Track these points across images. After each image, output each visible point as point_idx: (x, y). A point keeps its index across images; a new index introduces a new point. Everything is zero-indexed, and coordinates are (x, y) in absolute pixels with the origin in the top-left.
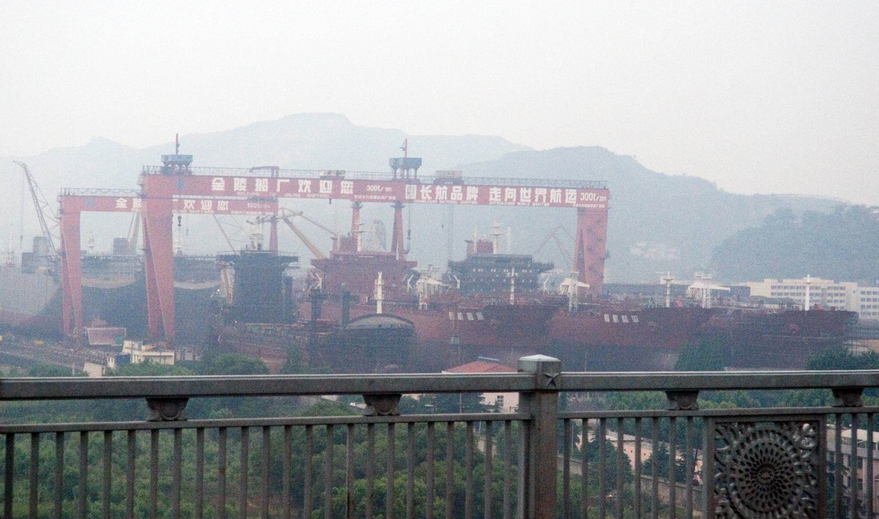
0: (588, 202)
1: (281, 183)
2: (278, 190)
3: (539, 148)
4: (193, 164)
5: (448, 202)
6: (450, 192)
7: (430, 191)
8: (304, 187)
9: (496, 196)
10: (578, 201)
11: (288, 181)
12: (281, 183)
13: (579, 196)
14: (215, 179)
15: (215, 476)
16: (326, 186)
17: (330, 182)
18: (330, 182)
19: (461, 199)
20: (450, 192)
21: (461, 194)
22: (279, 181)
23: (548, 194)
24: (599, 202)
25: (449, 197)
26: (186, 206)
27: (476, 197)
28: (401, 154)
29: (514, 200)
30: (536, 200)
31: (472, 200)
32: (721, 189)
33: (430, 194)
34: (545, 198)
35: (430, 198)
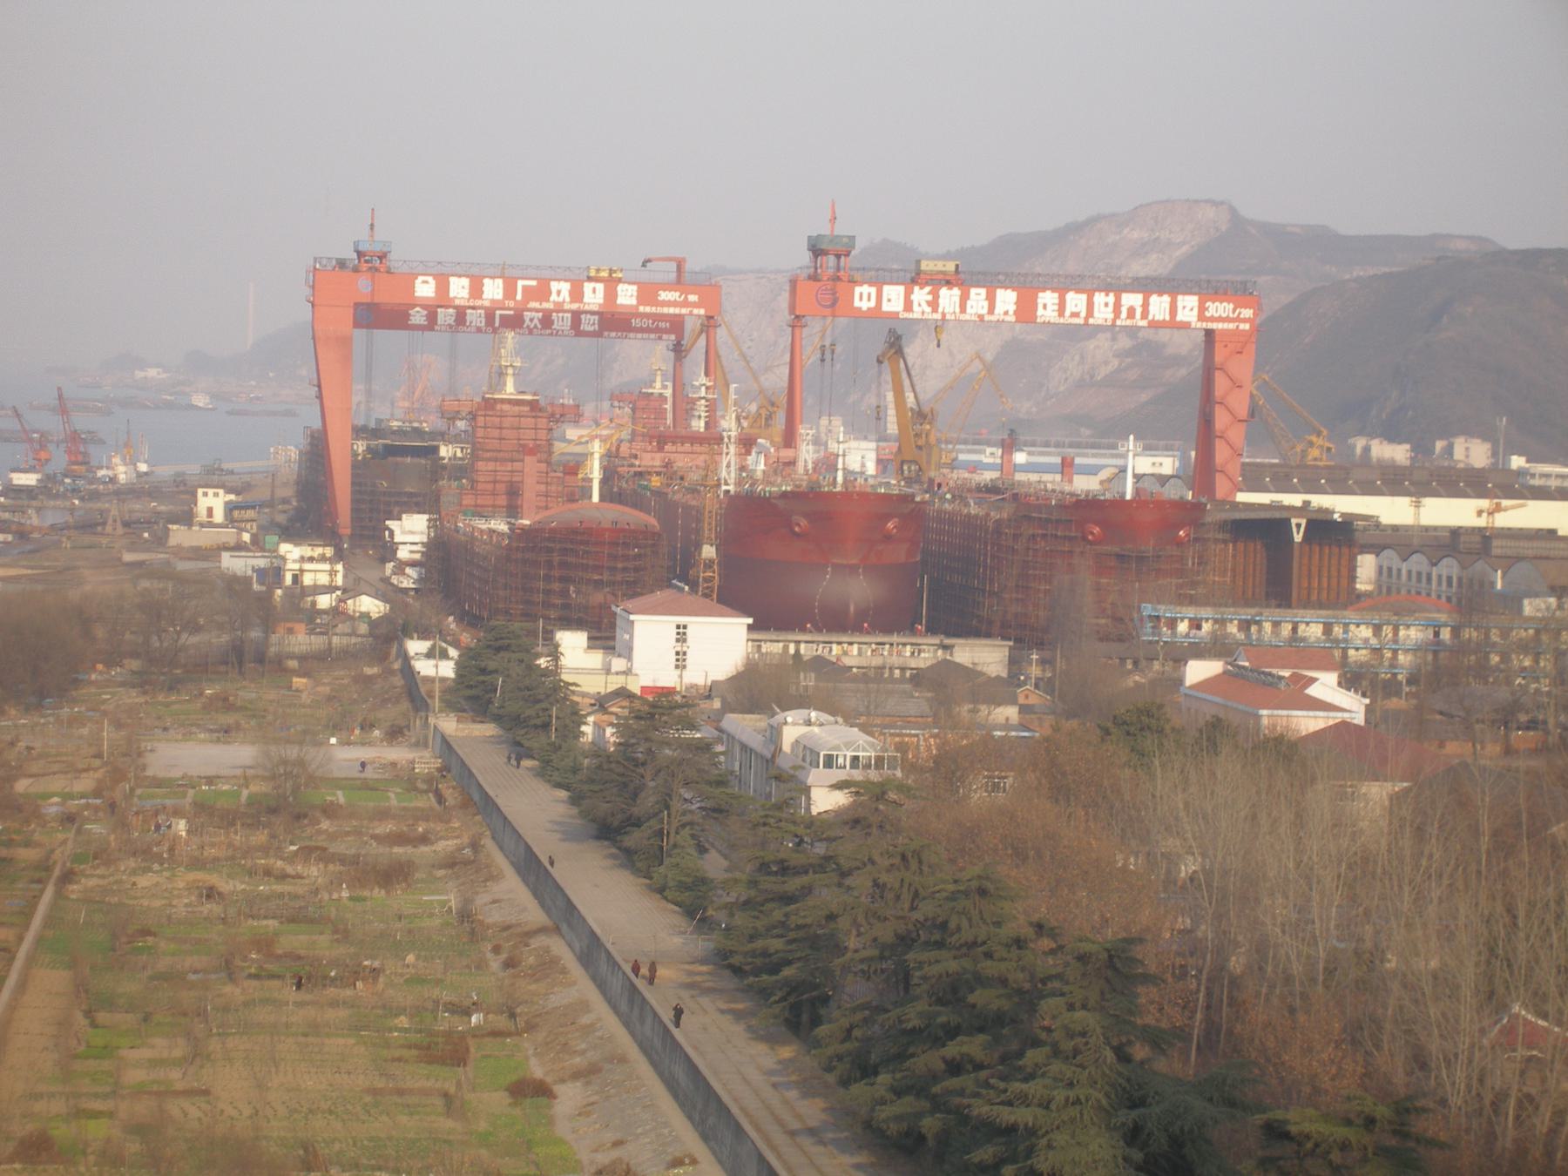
0: (1220, 319)
1: (525, 288)
2: (519, 297)
3: (1343, 231)
4: (392, 256)
5: (963, 317)
6: (964, 298)
7: (930, 298)
8: (559, 293)
9: (1050, 307)
10: (1201, 317)
11: (534, 283)
12: (525, 288)
13: (1202, 309)
14: (421, 279)
15: (301, 628)
16: (594, 291)
17: (600, 287)
18: (600, 287)
19: (985, 311)
20: (964, 298)
21: (986, 304)
22: (520, 283)
23: (1146, 305)
24: (1238, 320)
25: (963, 309)
26: (527, 322)
27: (1012, 308)
28: (825, 230)
29: (1083, 314)
30: (1124, 314)
31: (1006, 313)
32: (1379, 460)
33: (929, 303)
34: (1139, 311)
35: (929, 309)
